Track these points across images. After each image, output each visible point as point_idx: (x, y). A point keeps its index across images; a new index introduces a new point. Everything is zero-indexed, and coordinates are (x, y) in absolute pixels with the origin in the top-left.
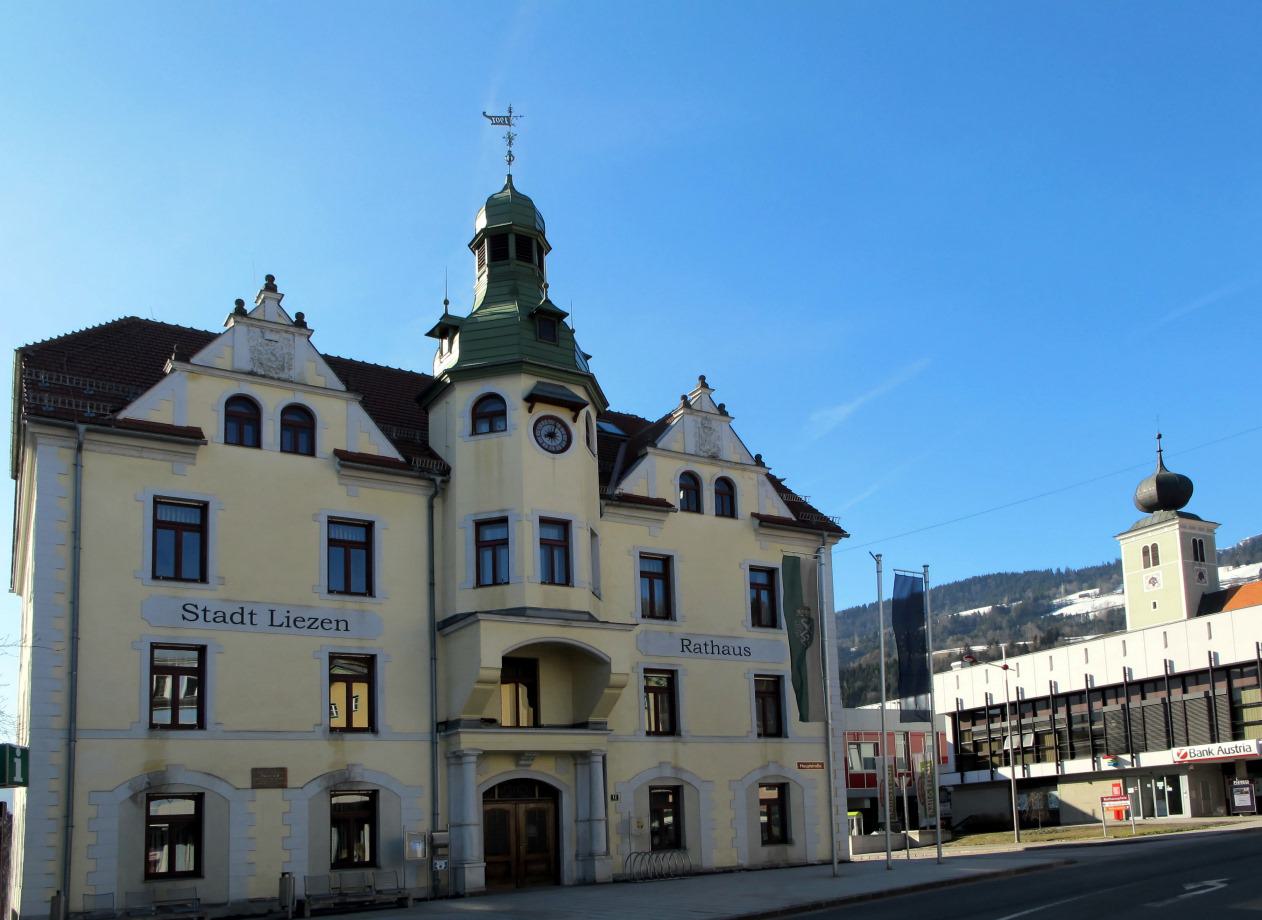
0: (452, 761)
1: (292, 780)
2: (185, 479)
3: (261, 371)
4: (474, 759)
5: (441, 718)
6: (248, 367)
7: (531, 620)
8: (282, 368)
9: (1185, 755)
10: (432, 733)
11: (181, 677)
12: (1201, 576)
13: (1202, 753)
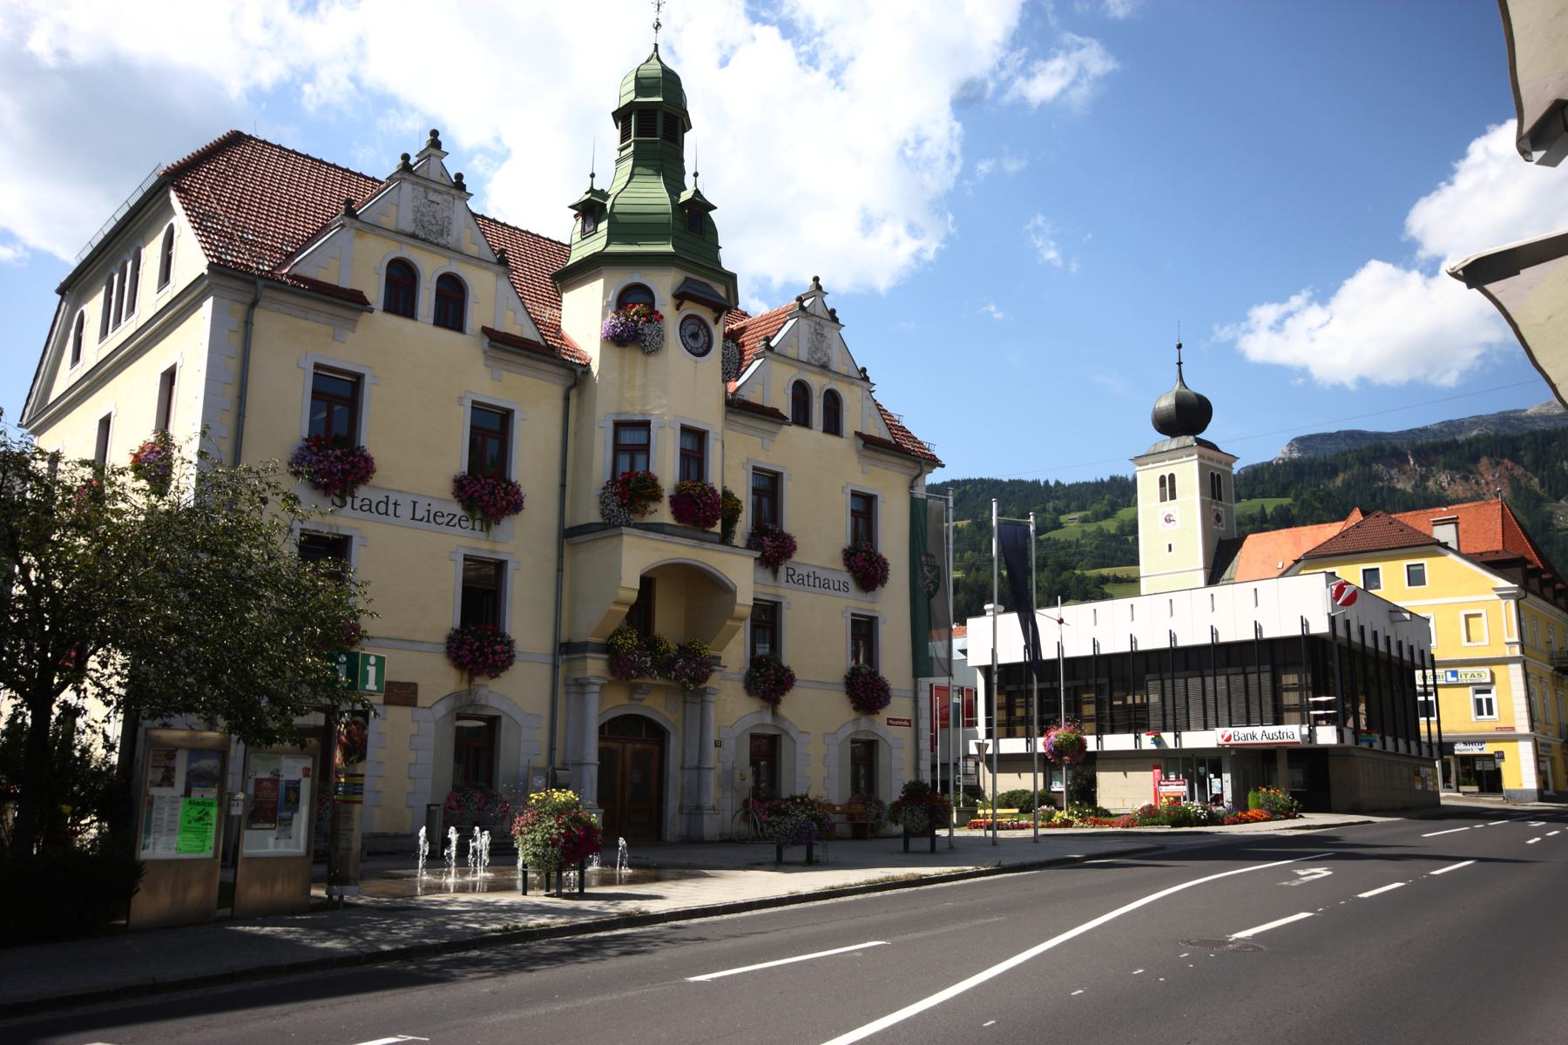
0: (572, 689)
1: (422, 700)
2: (350, 348)
3: (422, 234)
4: (597, 688)
5: (564, 639)
6: (410, 228)
7: (669, 538)
8: (441, 233)
9: (1229, 739)
10: (554, 655)
11: (1443, 802)
12: (1218, 518)
13: (1246, 737)
